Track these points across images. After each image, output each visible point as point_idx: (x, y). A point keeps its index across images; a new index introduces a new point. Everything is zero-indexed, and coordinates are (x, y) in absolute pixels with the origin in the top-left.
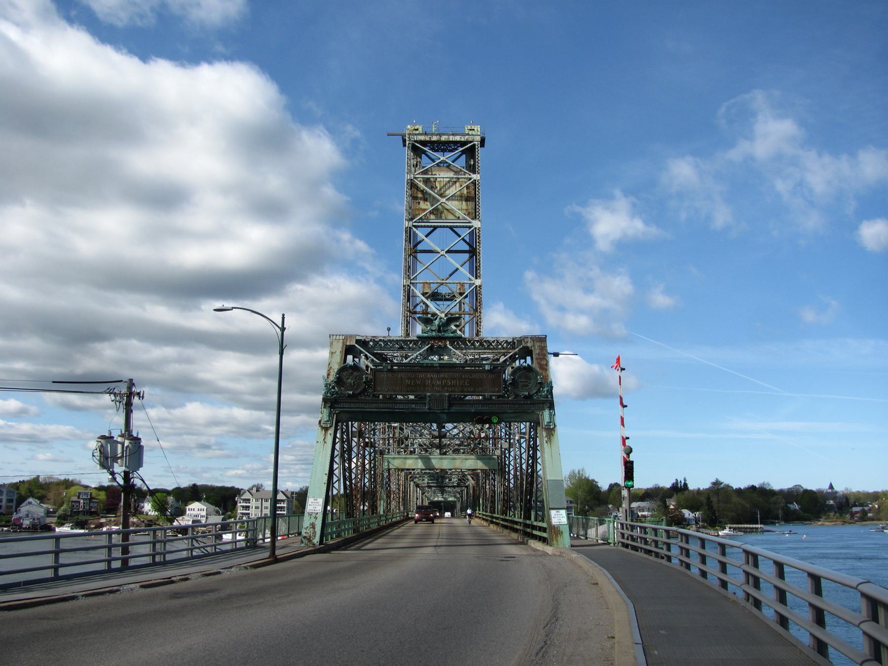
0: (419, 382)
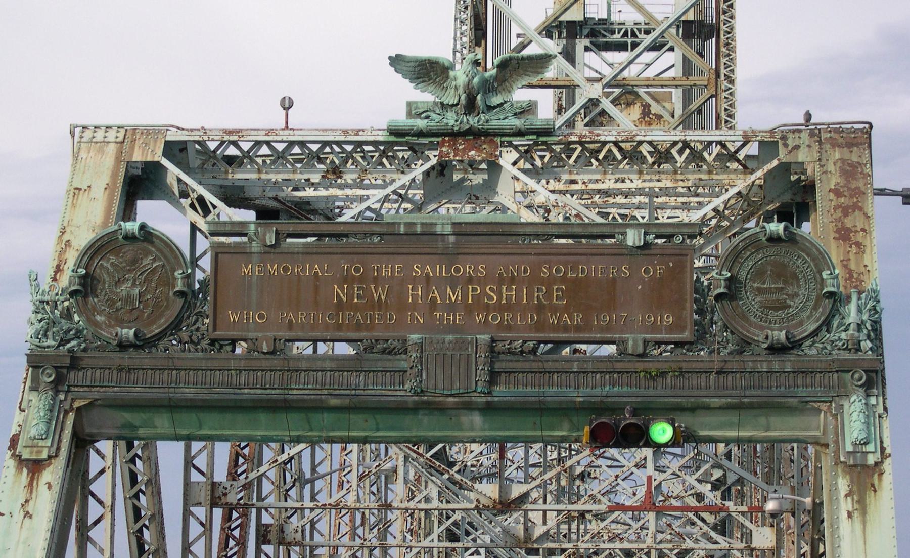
0: (379, 293)
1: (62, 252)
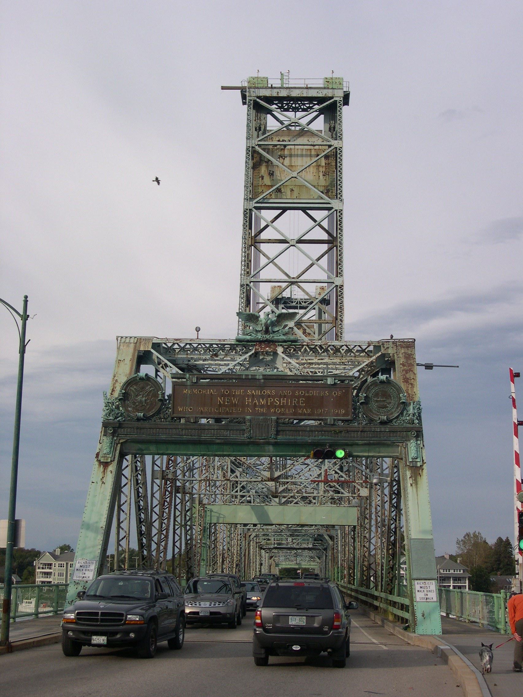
0: (235, 401)
1: (114, 384)
